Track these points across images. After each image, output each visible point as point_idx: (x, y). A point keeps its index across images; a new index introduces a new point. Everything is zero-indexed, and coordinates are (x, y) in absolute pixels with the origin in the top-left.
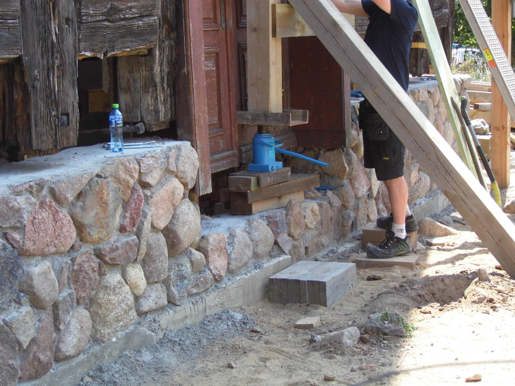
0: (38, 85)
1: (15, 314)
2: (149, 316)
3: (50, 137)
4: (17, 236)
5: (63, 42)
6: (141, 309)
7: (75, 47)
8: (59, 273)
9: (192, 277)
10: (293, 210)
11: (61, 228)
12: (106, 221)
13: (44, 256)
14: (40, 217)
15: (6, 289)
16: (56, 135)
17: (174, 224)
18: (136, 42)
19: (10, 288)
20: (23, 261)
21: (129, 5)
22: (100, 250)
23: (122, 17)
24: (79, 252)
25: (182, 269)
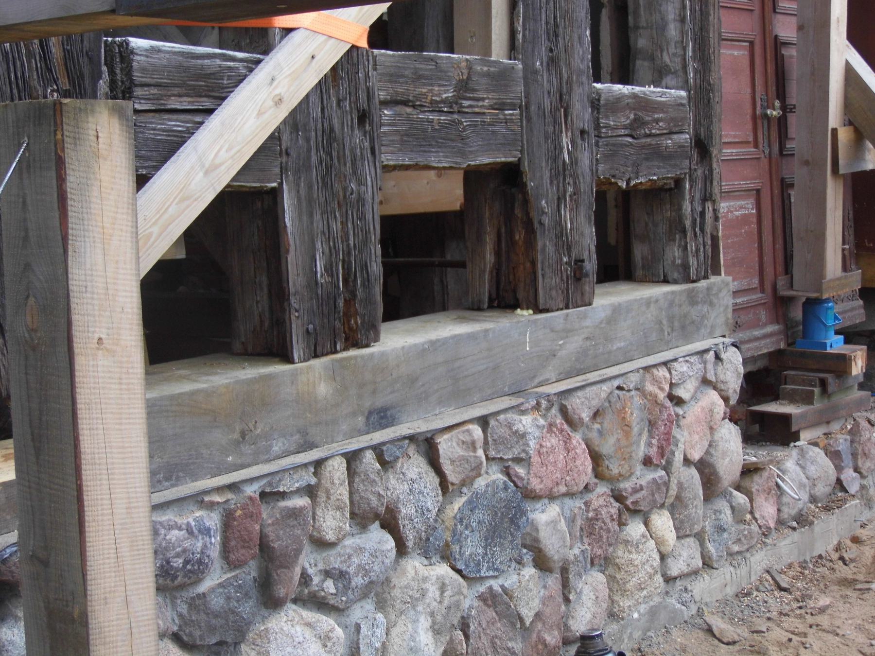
0: (546, 220)
1: (515, 578)
2: (678, 583)
3: (560, 292)
4: (521, 471)
5: (576, 163)
6: (669, 572)
7: (592, 170)
8: (571, 521)
9: (733, 529)
10: (861, 436)
11: (574, 459)
12: (629, 450)
13: (552, 497)
14: (549, 445)
15: (506, 543)
16: (567, 290)
17: (712, 455)
18: (664, 168)
19: (512, 542)
20: (528, 506)
21: (656, 116)
22: (620, 491)
23: (648, 132)
24: (594, 493)
25: (721, 517)
